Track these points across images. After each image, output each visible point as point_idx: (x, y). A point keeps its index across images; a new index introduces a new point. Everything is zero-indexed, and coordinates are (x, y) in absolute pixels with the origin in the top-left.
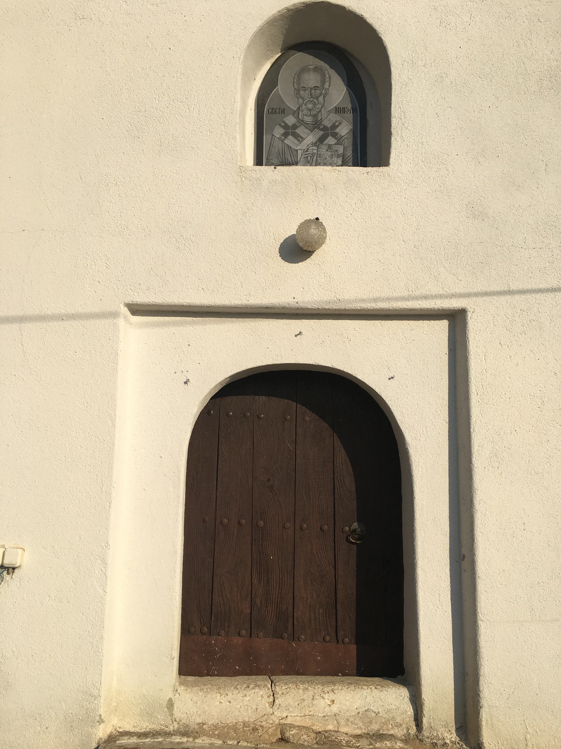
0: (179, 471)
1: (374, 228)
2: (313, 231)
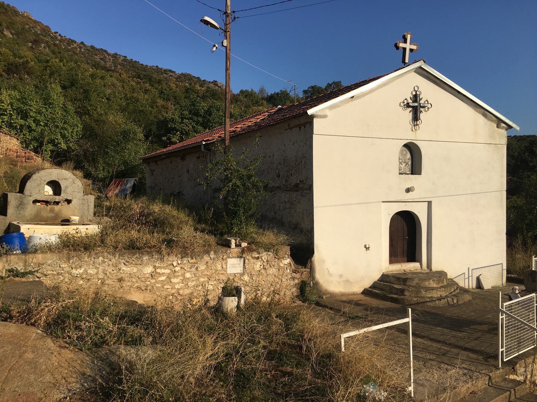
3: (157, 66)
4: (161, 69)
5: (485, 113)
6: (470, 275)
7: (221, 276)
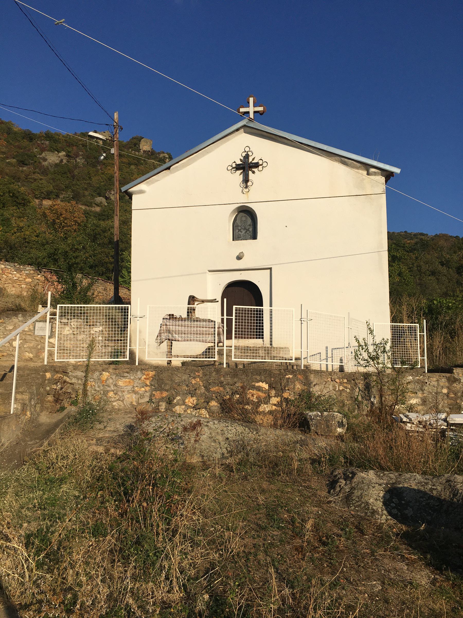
0: (189, 160)
1: (253, 252)
2: (241, 255)
3: (405, 232)
4: (410, 234)
5: (343, 160)
6: (330, 355)
7: (28, 336)
